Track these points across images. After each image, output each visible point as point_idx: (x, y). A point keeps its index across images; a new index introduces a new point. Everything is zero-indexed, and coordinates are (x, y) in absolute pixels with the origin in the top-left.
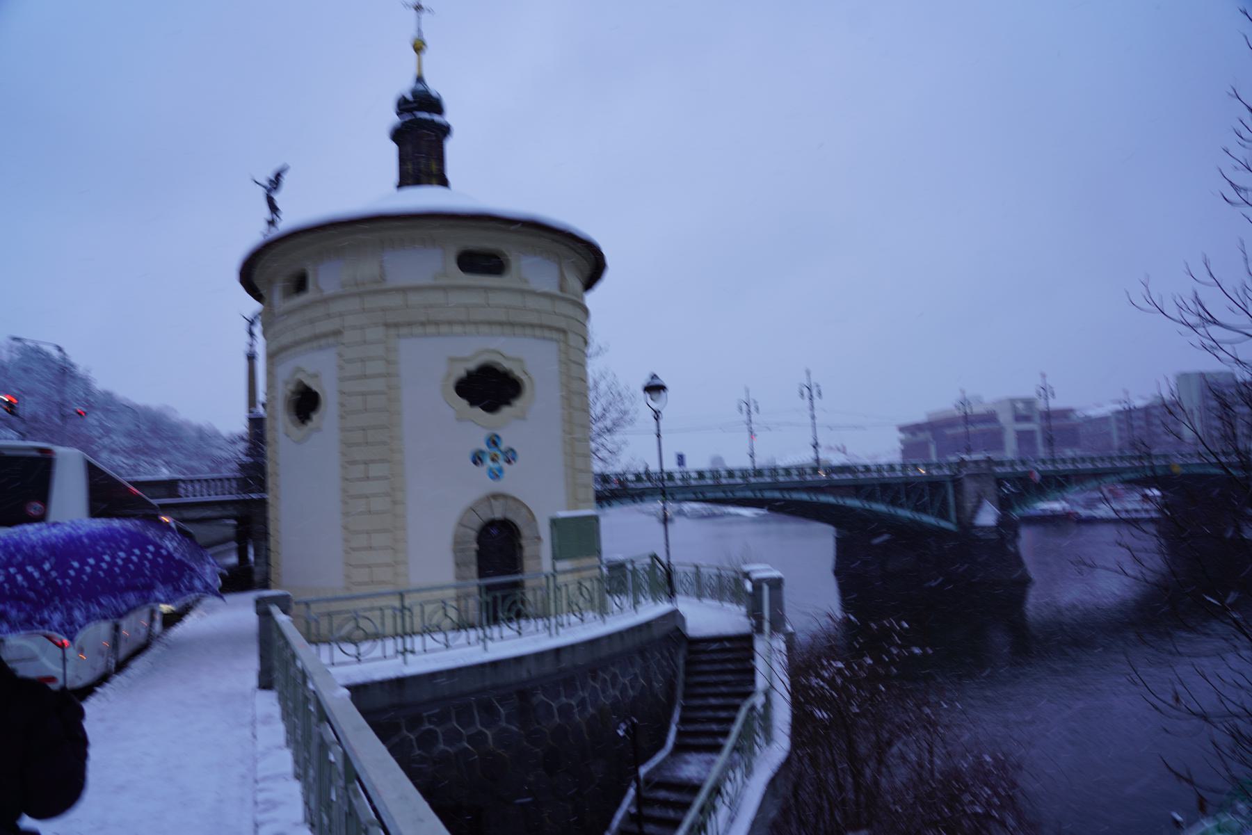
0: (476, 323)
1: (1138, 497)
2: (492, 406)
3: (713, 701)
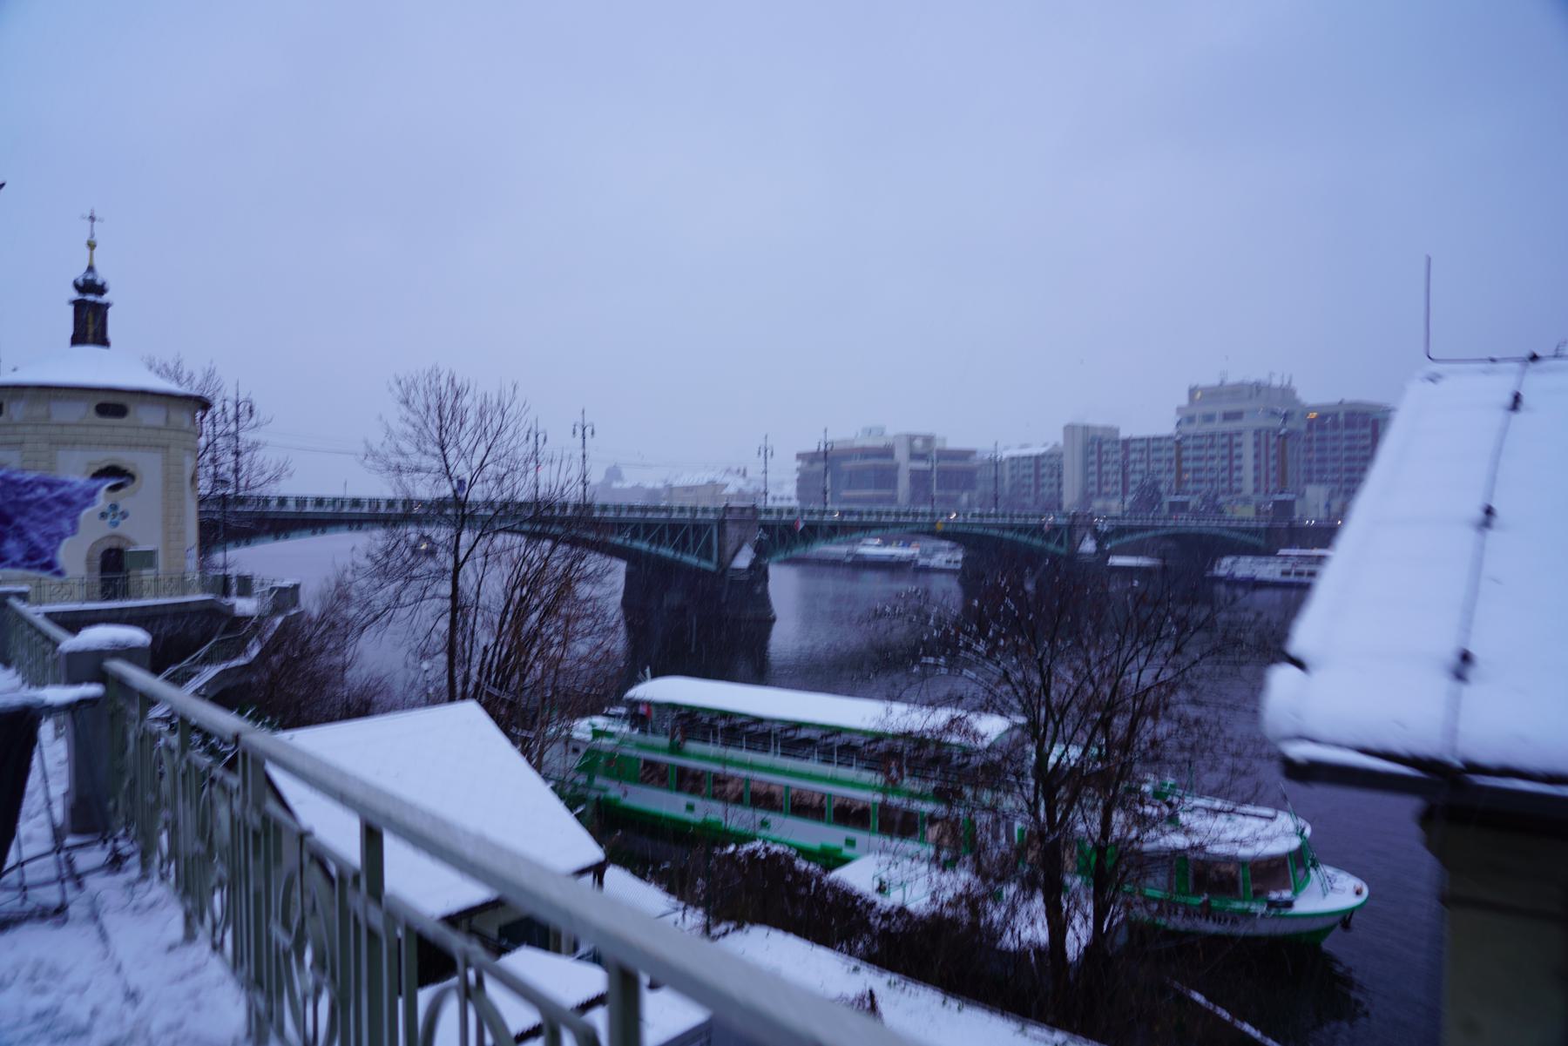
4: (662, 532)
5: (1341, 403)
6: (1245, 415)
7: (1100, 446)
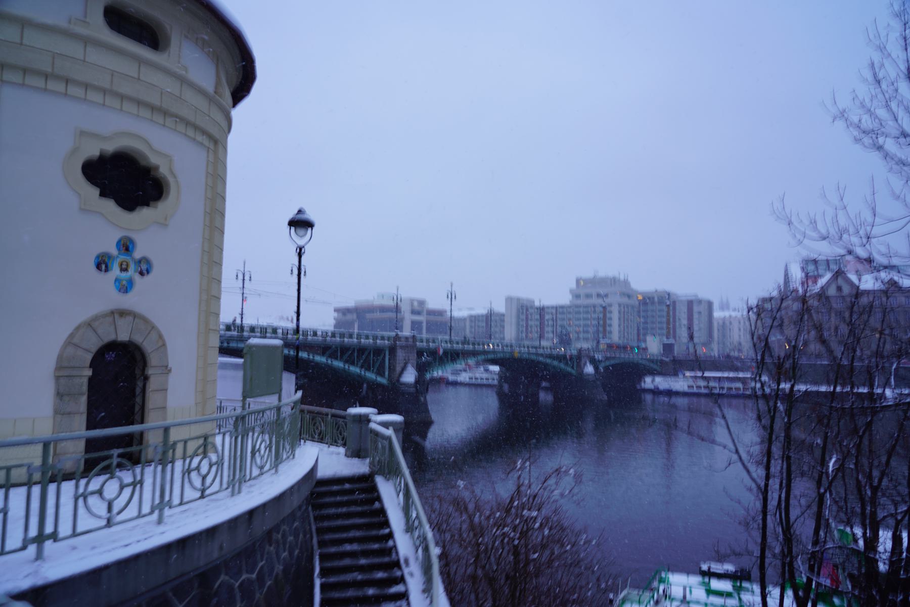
0: (122, 97)
1: (482, 369)
2: (129, 202)
3: (348, 547)
4: (336, 351)
5: (656, 291)
6: (609, 296)
7: (527, 310)
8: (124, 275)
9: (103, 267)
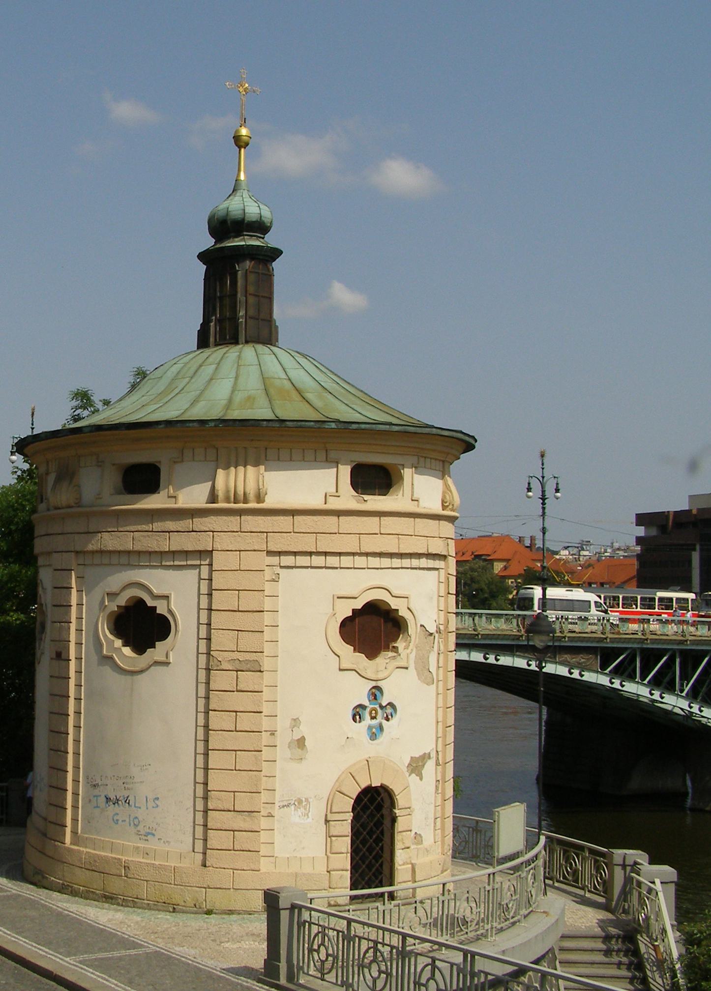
8: (374, 722)
9: (358, 717)
